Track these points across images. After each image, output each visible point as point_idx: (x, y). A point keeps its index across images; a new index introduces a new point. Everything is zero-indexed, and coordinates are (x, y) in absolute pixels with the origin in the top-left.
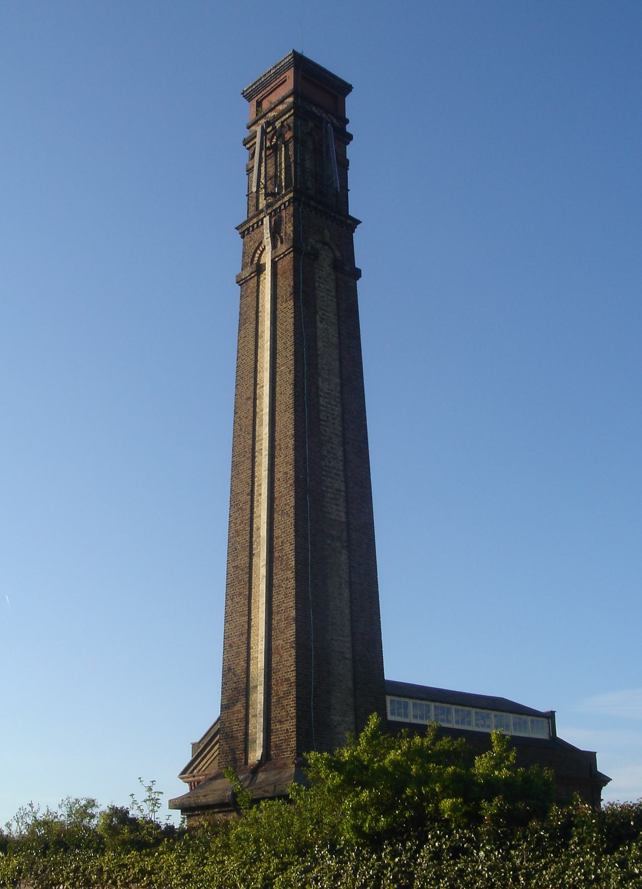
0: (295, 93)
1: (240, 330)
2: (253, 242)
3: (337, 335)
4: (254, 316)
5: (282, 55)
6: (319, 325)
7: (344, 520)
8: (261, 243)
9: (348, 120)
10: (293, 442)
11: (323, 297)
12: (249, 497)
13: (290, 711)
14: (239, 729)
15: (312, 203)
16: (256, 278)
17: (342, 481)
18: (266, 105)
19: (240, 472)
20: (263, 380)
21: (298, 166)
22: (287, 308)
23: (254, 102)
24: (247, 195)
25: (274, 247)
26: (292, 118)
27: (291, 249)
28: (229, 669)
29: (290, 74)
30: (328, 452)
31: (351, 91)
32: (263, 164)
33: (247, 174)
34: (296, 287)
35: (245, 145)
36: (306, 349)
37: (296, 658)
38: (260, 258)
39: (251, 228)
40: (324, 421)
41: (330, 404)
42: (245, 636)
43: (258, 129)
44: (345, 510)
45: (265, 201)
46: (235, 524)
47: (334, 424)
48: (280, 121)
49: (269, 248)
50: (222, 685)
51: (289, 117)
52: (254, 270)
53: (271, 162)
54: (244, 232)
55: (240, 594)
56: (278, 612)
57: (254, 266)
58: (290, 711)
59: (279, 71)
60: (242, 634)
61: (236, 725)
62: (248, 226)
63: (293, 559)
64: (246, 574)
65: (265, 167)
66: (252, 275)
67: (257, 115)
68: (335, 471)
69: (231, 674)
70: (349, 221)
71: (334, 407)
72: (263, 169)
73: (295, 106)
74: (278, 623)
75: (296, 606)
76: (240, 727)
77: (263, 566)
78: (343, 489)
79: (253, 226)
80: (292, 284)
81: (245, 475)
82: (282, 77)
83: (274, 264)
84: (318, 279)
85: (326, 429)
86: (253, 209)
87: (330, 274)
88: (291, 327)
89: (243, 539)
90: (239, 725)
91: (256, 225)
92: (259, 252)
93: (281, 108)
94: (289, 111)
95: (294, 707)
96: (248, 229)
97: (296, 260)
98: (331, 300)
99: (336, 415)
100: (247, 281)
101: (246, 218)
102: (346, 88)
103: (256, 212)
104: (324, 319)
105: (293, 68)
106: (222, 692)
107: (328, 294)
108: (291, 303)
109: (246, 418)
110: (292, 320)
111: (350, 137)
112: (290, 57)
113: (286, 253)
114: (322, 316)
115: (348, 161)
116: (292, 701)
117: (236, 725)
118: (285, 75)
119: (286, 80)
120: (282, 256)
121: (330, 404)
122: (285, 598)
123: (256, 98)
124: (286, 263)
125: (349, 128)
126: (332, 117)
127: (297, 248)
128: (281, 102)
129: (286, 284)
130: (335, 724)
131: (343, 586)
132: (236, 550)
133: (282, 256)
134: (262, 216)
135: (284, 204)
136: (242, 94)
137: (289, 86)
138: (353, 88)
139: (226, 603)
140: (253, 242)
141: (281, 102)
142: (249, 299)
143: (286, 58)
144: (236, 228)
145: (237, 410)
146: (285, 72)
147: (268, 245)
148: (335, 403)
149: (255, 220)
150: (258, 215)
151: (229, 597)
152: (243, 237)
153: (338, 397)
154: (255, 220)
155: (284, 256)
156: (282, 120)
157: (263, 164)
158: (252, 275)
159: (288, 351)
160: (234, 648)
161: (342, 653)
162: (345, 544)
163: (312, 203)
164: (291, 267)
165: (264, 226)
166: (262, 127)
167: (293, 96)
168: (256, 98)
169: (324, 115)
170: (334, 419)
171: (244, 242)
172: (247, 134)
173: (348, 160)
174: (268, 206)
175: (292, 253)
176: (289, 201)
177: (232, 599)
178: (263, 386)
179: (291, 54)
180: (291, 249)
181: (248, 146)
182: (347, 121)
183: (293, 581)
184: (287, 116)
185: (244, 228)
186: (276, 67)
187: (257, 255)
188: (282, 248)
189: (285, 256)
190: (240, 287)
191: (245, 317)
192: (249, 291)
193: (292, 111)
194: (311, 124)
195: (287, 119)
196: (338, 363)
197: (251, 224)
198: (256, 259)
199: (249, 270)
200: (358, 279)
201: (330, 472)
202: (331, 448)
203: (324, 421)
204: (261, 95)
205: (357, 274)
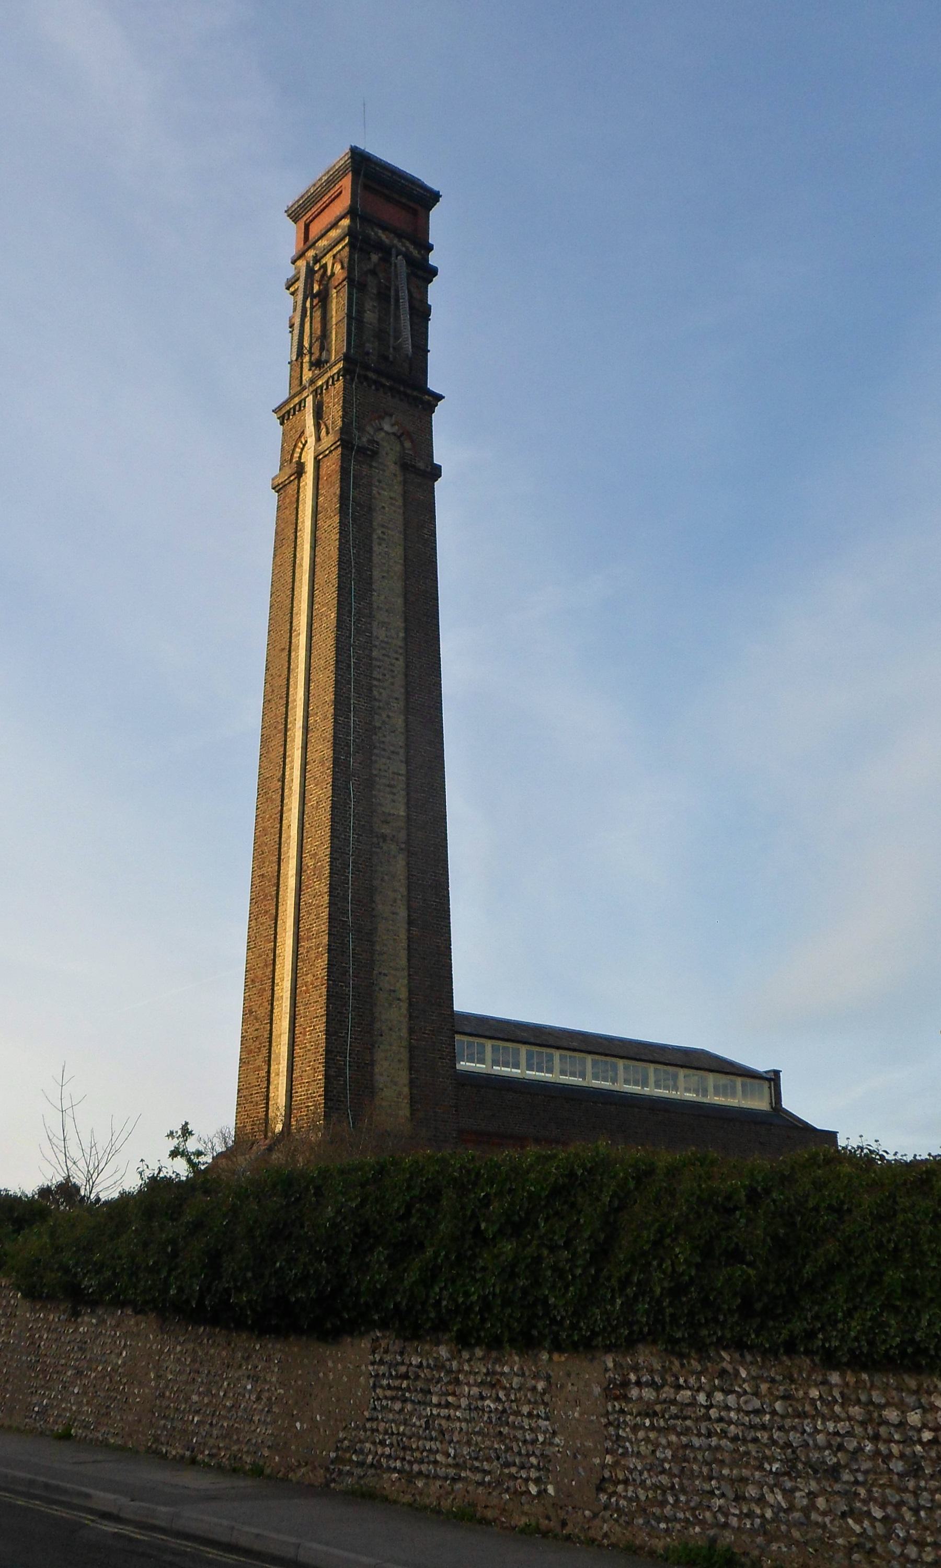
0: (352, 212)
1: (275, 555)
2: (294, 430)
3: (401, 561)
4: (292, 537)
5: (338, 155)
6: (376, 548)
7: (402, 813)
8: (303, 432)
9: (433, 246)
10: (333, 711)
11: (383, 507)
12: (280, 783)
13: (318, 1068)
14: (259, 1091)
15: (371, 375)
16: (296, 482)
17: (402, 762)
18: (315, 230)
19: (271, 749)
20: (284, 956)
21: (354, 321)
22: (331, 524)
23: (302, 223)
24: (289, 363)
25: (318, 439)
26: (347, 249)
27: (338, 443)
28: (251, 1012)
29: (347, 182)
30: (384, 722)
31: (438, 201)
32: (308, 319)
33: (290, 332)
34: (343, 498)
35: (288, 288)
36: (355, 583)
37: (327, 999)
38: (300, 457)
39: (292, 411)
40: (379, 680)
41: (389, 657)
42: (270, 969)
43: (302, 263)
44: (406, 801)
45: (311, 372)
46: (263, 818)
47: (392, 684)
48: (331, 254)
49: (311, 441)
50: (242, 1033)
51: (343, 247)
52: (293, 471)
53: (318, 314)
54: (283, 417)
55: (266, 912)
56: (309, 939)
57: (294, 465)
58: (318, 1068)
59: (332, 179)
60: (266, 965)
61: (256, 1086)
62: (287, 408)
63: (328, 867)
64: (274, 886)
65: (311, 323)
66: (292, 478)
67: (305, 243)
68: (392, 748)
69: (252, 1018)
70: (427, 397)
71: (394, 661)
72: (307, 326)
73: (351, 232)
74: (308, 952)
75: (329, 930)
76: (261, 1089)
77: (292, 876)
78: (403, 772)
79: (294, 407)
80: (338, 492)
81: (276, 754)
82: (337, 187)
83: (317, 462)
84: (377, 484)
85: (381, 690)
86: (297, 382)
87: (395, 475)
88: (335, 554)
89: (271, 839)
90: (259, 1085)
91: (297, 408)
92: (301, 446)
93: (334, 234)
94: (342, 239)
95: (322, 1063)
96: (288, 412)
97: (344, 458)
98: (395, 512)
99: (396, 672)
100: (286, 485)
101: (287, 396)
102: (435, 197)
103: (299, 388)
104: (384, 539)
105: (350, 173)
106: (242, 1041)
107: (392, 504)
108: (337, 519)
109: (280, 676)
110: (337, 543)
111: (433, 272)
112: (346, 158)
113: (332, 448)
114: (381, 535)
115: (429, 308)
116: (321, 1055)
117: (256, 1086)
118: (340, 183)
119: (341, 193)
120: (327, 452)
121: (389, 657)
122: (317, 918)
123: (305, 218)
124: (332, 465)
125: (433, 259)
126: (408, 244)
127: (346, 442)
128: (334, 225)
129: (331, 491)
130: (381, 1086)
131: (399, 902)
132: (263, 854)
133: (327, 452)
134: (305, 394)
135: (333, 377)
136: (286, 212)
137: (345, 202)
138: (441, 196)
139: (249, 925)
140: (294, 430)
141: (334, 225)
142: (287, 512)
143: (341, 159)
144: (273, 411)
145: (270, 665)
146: (341, 180)
147: (292, 876)
148: (396, 656)
149: (296, 400)
150: (300, 392)
151: (254, 917)
152: (282, 423)
153: (400, 647)
154: (296, 400)
155: (330, 452)
156: (335, 252)
157: (308, 319)
158: (292, 478)
159: (331, 586)
160: (257, 984)
161: (394, 991)
162: (403, 846)
163: (371, 375)
164: (338, 468)
165: (307, 409)
166: (308, 263)
167: (349, 216)
168: (305, 218)
169: (396, 241)
170: (393, 677)
171: (284, 430)
172: (290, 271)
173: (430, 306)
174: (312, 382)
175: (340, 449)
176: (338, 373)
177: (256, 919)
178: (299, 634)
179: (347, 154)
180: (338, 443)
181: (292, 289)
182: (430, 248)
183: (326, 898)
184: (341, 247)
185: (284, 411)
186: (328, 172)
187: (298, 450)
188: (328, 440)
189: (331, 452)
190: (277, 494)
191: (282, 537)
192: (288, 500)
193: (347, 241)
194: (375, 258)
195: (339, 252)
196: (406, 952)
197: (292, 406)
198: (296, 455)
199: (288, 470)
200: (431, 281)
201: (384, 750)
202: (388, 716)
203: (379, 680)
204: (310, 213)
205: (435, 472)
